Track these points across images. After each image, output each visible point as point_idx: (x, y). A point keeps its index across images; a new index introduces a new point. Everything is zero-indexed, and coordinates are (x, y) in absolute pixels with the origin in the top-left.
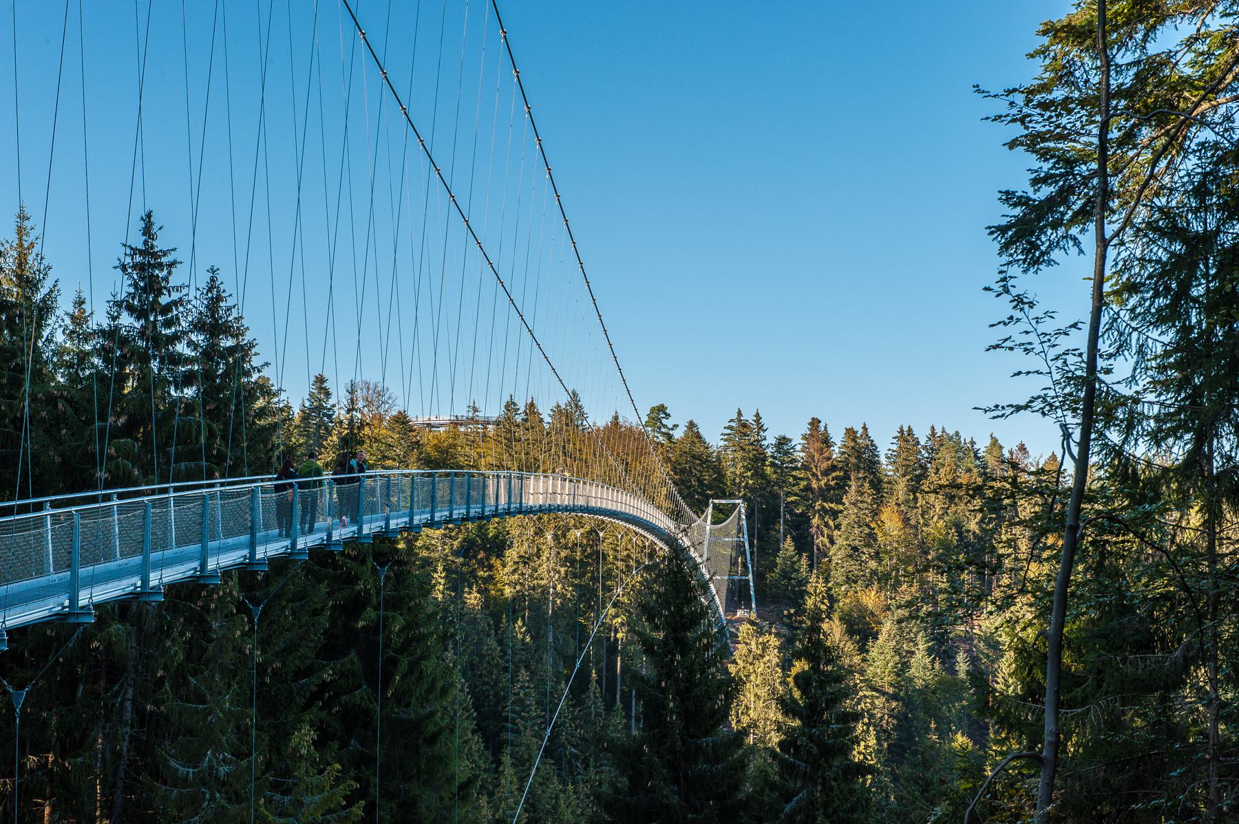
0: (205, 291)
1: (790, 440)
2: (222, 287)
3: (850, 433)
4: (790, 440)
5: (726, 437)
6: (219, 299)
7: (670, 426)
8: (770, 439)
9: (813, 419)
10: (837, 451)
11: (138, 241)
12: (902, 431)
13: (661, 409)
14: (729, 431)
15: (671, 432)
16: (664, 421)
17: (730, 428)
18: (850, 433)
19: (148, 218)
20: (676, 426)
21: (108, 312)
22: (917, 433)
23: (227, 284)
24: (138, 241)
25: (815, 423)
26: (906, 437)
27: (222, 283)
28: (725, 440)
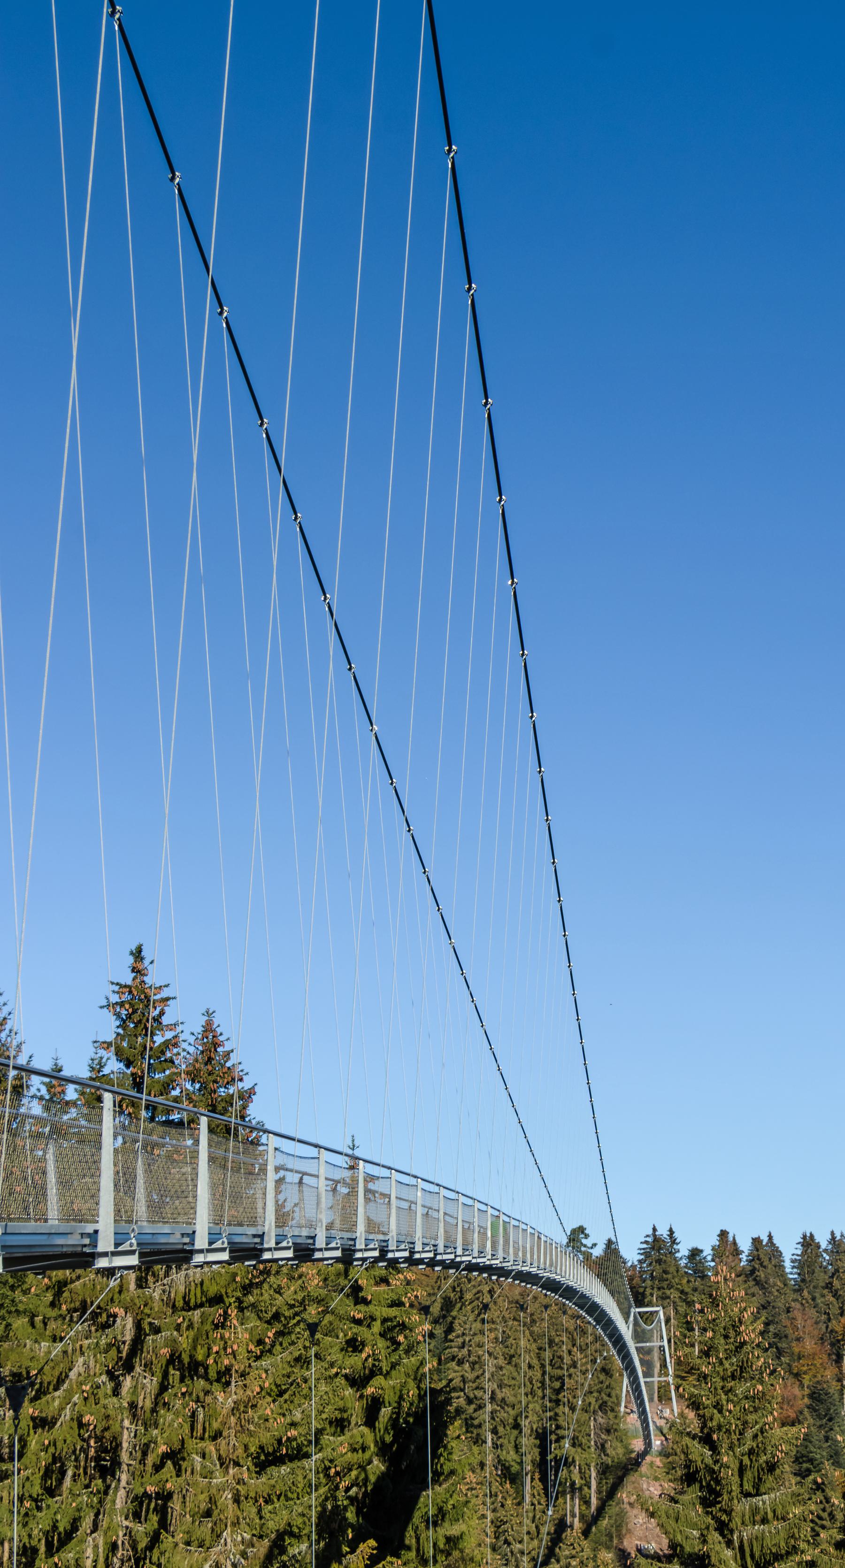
0: (200, 1036)
1: (701, 1251)
2: (219, 1030)
3: (756, 1241)
4: (701, 1251)
5: (642, 1251)
6: (216, 1045)
7: (590, 1245)
8: (683, 1251)
9: (722, 1231)
10: (745, 1259)
11: (127, 978)
12: (804, 1237)
13: (581, 1229)
14: (645, 1246)
15: (590, 1251)
16: (584, 1241)
17: (646, 1242)
18: (756, 1241)
19: (138, 954)
20: (595, 1245)
21: (89, 1066)
22: (818, 1238)
23: (225, 1027)
24: (127, 978)
25: (723, 1234)
26: (808, 1242)
27: (219, 1026)
28: (642, 1254)
